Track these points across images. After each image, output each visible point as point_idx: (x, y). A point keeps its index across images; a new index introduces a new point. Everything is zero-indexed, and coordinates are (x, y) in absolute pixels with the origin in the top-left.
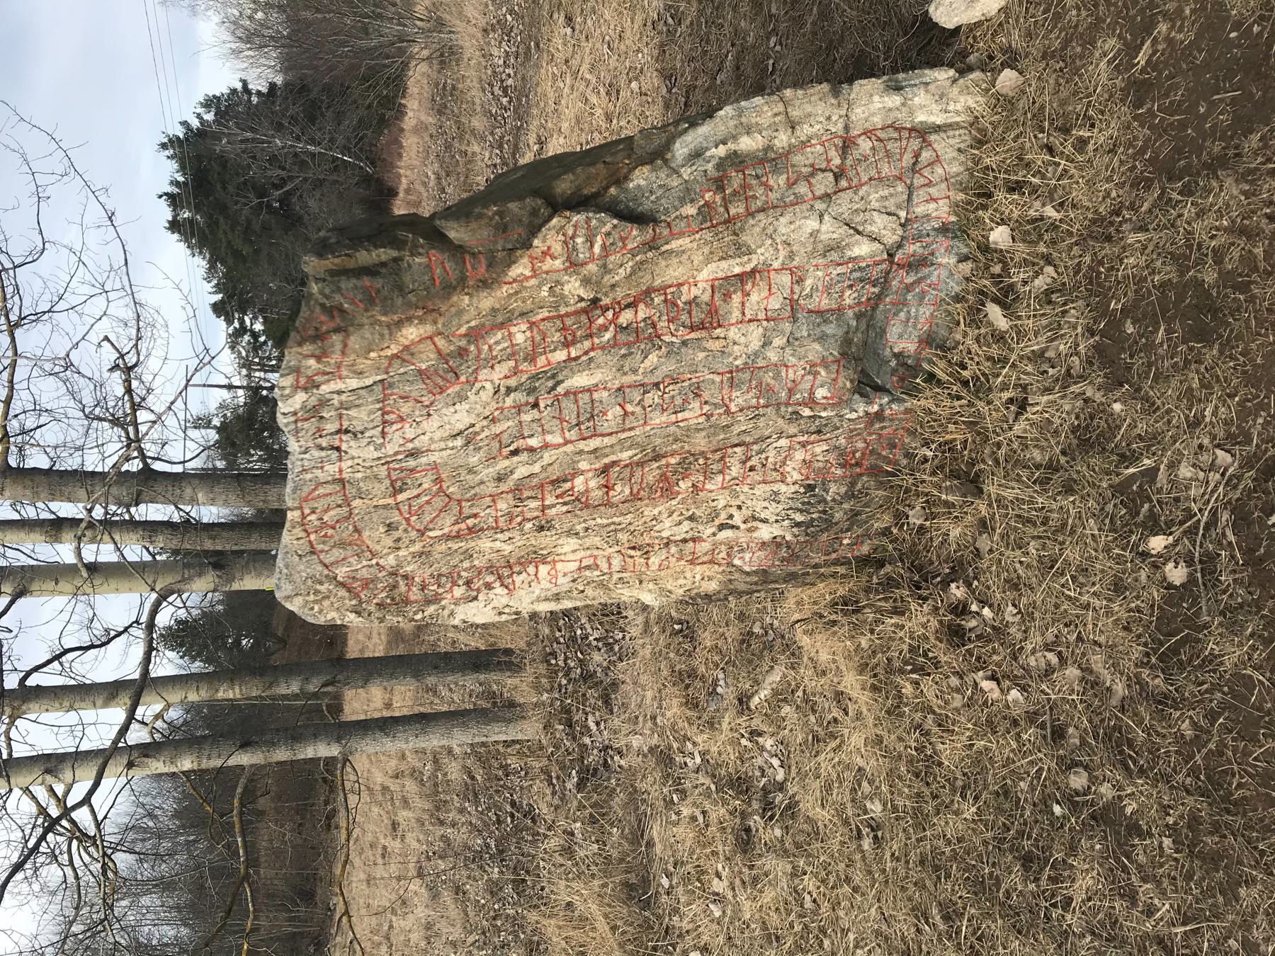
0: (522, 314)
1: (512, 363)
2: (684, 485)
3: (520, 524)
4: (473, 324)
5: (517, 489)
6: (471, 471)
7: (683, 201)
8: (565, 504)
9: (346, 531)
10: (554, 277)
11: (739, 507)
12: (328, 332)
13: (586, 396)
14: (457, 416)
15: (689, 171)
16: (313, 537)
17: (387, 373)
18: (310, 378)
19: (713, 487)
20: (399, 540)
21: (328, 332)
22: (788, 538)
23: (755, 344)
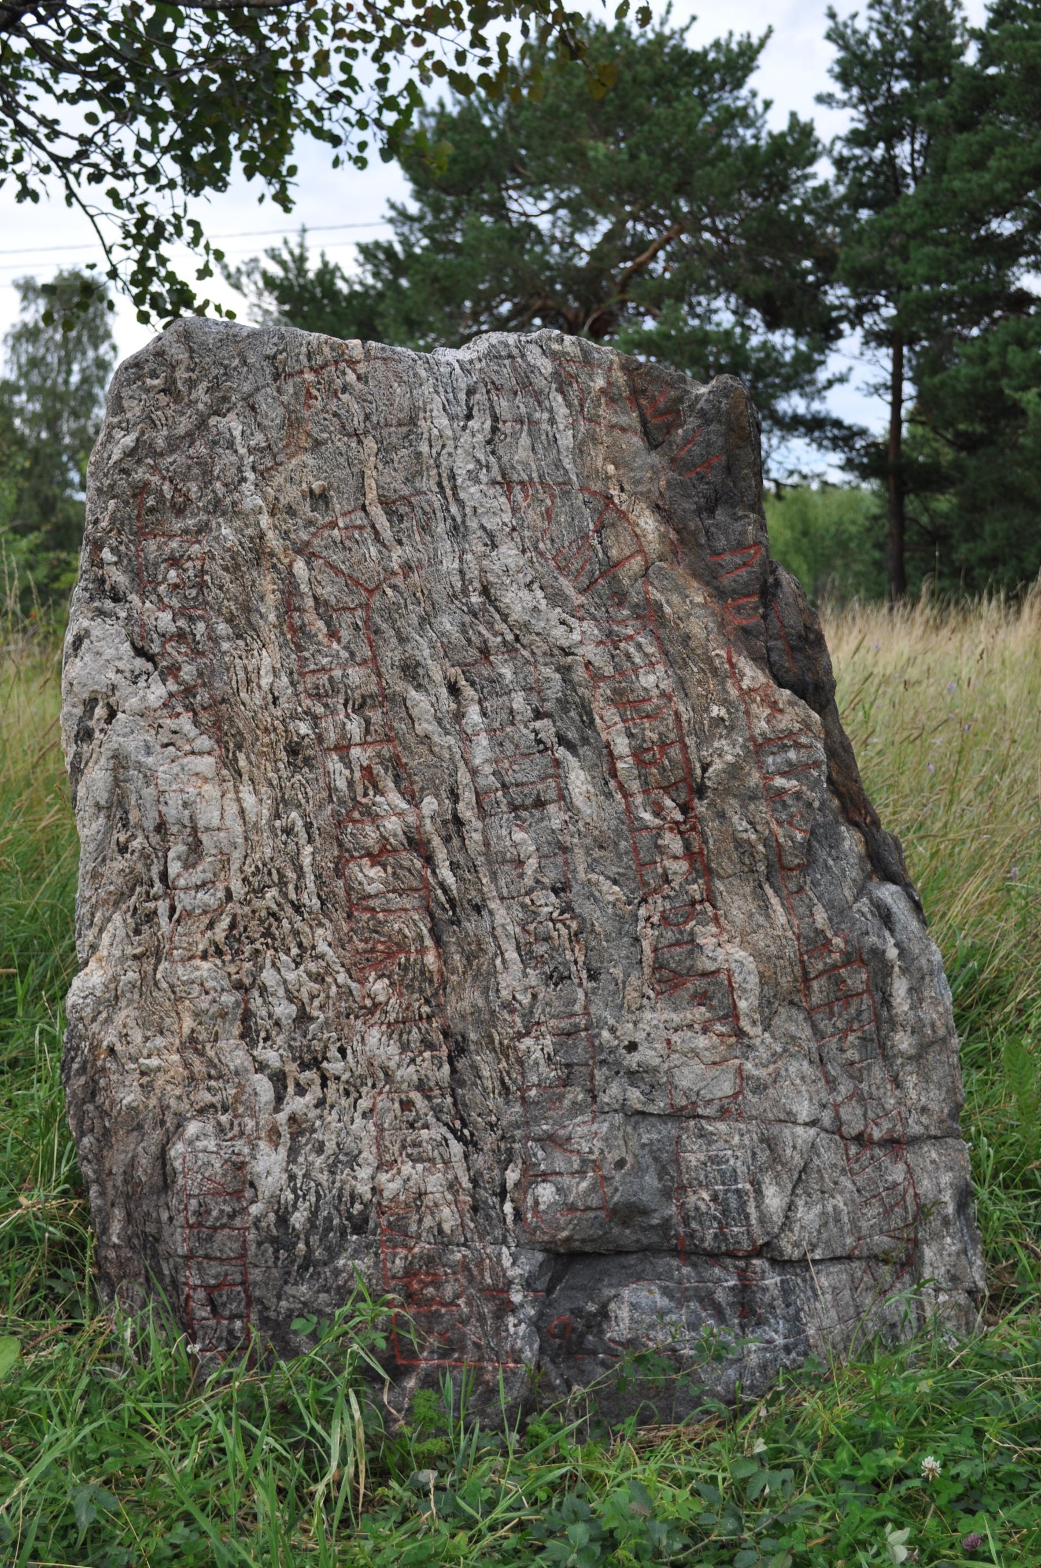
1: (609, 670)
4: (667, 610)
5: (387, 699)
7: (829, 906)
8: (351, 783)
10: (742, 722)
11: (321, 1103)
12: (639, 407)
15: (865, 910)
16: (309, 377)
17: (581, 490)
20: (291, 511)
21: (639, 407)
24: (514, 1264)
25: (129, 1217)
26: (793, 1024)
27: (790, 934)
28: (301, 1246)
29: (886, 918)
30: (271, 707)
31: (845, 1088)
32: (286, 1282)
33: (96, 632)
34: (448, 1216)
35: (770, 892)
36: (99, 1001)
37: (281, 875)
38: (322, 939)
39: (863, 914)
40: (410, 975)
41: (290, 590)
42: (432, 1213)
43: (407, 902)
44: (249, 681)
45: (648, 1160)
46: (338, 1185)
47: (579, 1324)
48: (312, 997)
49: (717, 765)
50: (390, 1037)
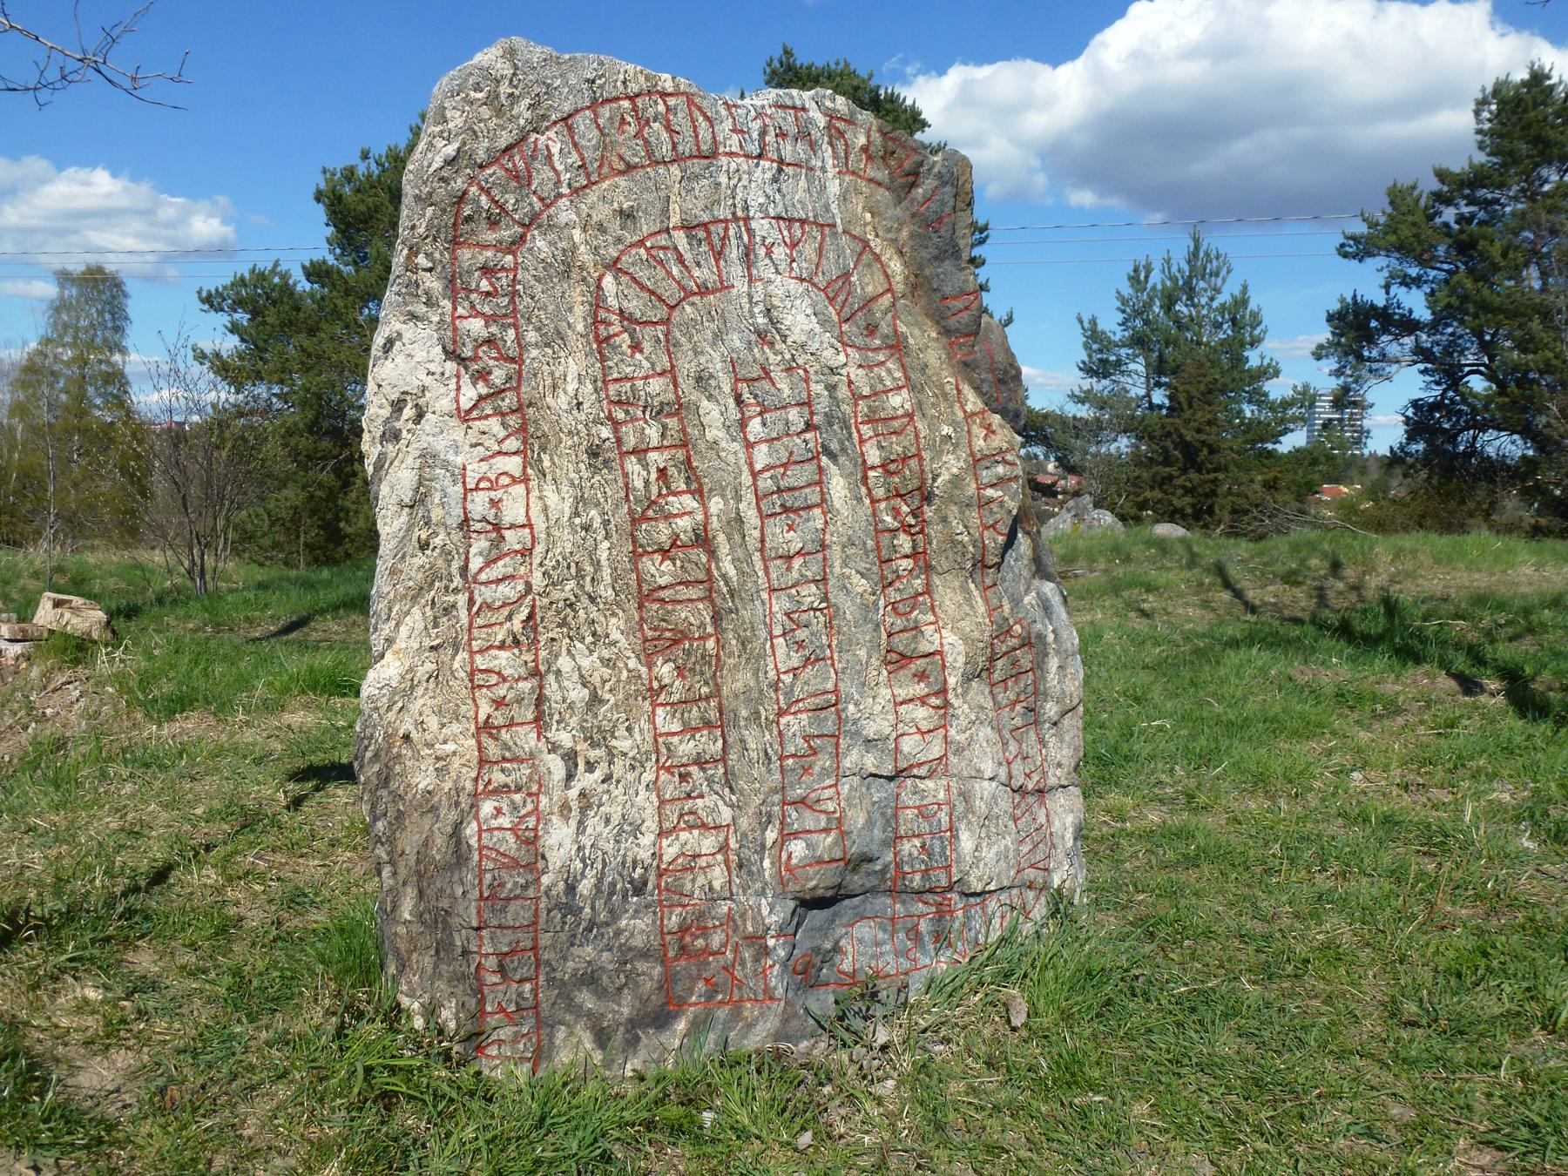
0: (920, 403)
2: (665, 670)
3: (610, 417)
4: (911, 341)
5: (679, 408)
6: (718, 337)
8: (647, 482)
9: (636, 155)
11: (607, 779)
13: (816, 498)
14: (801, 318)
16: (626, 104)
18: (841, 134)
19: (659, 721)
20: (601, 228)
22: (546, 880)
26: (979, 692)
28: (587, 910)
29: (1046, 607)
30: (575, 412)
32: (572, 945)
33: (407, 336)
34: (718, 877)
35: (972, 586)
36: (394, 692)
37: (579, 569)
41: (597, 302)
43: (694, 593)
44: (555, 387)
45: (877, 815)
47: (817, 960)
48: (604, 682)
49: (945, 477)
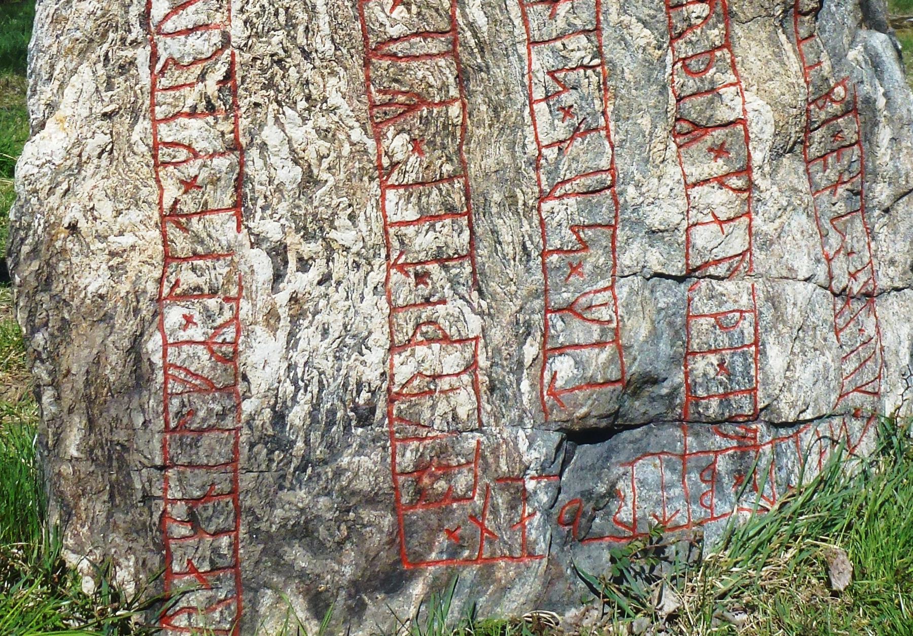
2: (398, 144)
11: (324, 280)
19: (390, 207)
22: (248, 407)
23: (655, 218)
24: (530, 446)
25: (91, 424)
27: (802, 81)
31: (834, 240)
32: (281, 488)
35: (783, 38)
36: (57, 171)
37: (290, 17)
38: (334, 90)
39: (858, 63)
40: (433, 130)
42: (448, 398)
43: (434, 46)
46: (343, 372)
47: (588, 507)
48: (321, 158)
50: (408, 201)
